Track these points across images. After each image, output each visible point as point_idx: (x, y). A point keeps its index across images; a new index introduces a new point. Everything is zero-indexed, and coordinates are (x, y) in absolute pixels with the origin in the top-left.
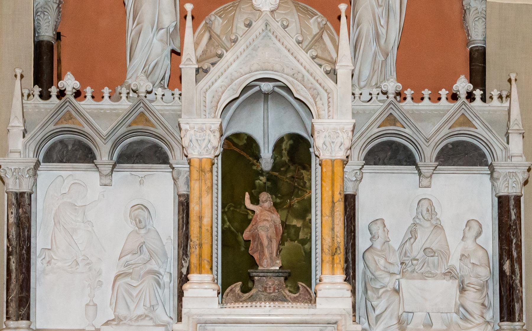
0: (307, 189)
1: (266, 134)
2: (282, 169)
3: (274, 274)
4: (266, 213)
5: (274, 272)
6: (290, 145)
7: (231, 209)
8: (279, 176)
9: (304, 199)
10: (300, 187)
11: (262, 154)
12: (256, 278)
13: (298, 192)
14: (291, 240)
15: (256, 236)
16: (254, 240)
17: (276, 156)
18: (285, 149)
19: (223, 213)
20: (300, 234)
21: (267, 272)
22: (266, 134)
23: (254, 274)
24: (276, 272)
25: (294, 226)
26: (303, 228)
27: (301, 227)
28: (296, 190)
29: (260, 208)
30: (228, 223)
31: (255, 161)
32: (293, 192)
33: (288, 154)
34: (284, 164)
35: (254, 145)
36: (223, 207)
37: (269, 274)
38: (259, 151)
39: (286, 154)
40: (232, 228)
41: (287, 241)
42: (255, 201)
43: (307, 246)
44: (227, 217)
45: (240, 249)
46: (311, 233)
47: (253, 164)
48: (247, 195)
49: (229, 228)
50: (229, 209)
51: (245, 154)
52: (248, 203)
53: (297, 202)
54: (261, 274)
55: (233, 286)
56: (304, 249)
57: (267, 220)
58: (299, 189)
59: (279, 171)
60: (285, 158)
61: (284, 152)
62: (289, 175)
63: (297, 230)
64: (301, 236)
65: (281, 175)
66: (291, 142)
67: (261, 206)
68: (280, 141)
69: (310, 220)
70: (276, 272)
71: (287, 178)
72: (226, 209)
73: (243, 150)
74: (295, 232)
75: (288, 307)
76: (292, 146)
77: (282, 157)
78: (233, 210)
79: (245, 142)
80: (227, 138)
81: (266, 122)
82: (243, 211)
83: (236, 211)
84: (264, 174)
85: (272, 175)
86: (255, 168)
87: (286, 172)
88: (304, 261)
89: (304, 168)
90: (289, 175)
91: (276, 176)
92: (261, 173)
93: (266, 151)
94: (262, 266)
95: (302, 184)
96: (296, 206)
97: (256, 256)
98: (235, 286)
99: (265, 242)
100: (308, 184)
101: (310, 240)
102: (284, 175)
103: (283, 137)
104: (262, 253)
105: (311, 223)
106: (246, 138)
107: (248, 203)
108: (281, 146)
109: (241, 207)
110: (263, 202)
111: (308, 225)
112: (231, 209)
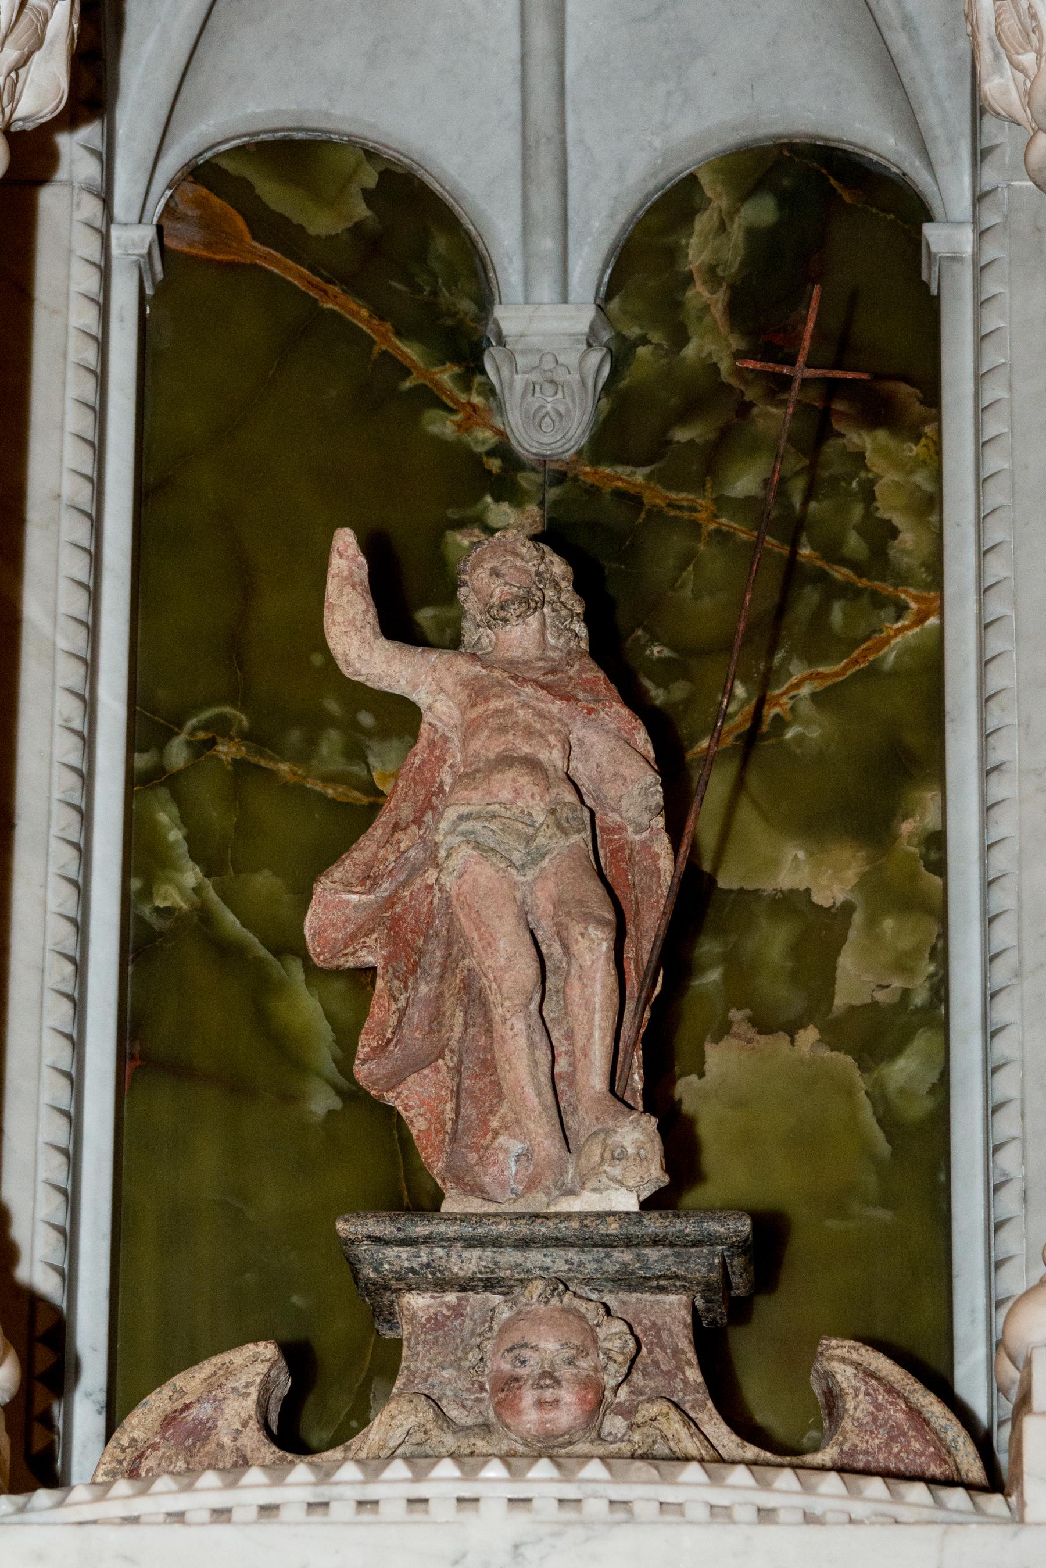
0: (902, 579)
1: (545, 152)
2: (681, 435)
3: (588, 1261)
4: (525, 702)
5: (588, 1235)
6: (751, 233)
7: (226, 750)
8: (657, 497)
9: (873, 672)
10: (840, 573)
11: (508, 317)
12: (418, 1303)
13: (822, 612)
14: (764, 1025)
15: (419, 934)
16: (407, 961)
17: (634, 332)
18: (711, 273)
19: (136, 783)
20: (847, 962)
21: (525, 1244)
22: (545, 152)
23: (398, 1257)
24: (608, 1243)
25: (793, 904)
26: (873, 921)
27: (848, 908)
28: (809, 597)
29: (465, 668)
30: (191, 876)
31: (446, 376)
32: (781, 610)
33: (733, 310)
34: (703, 394)
35: (441, 243)
36: (146, 728)
37: (535, 1257)
38: (485, 299)
39: (718, 311)
40: (231, 917)
41: (724, 1030)
42: (405, 607)
43: (904, 1070)
44: (185, 819)
45: (290, 1098)
46: (941, 954)
47: (429, 398)
48: (346, 556)
49: (204, 916)
50: (201, 749)
51: (359, 314)
52: (354, 640)
53: (815, 697)
54: (469, 1262)
55: (191, 1381)
56: (880, 1098)
57: (532, 764)
58: (833, 591)
59: (655, 452)
60: (712, 344)
61: (699, 293)
62: (745, 483)
63: (820, 933)
64: (856, 978)
65: (669, 480)
66: (762, 211)
67: (474, 657)
68: (674, 206)
69: (936, 842)
70: (608, 1243)
71: (722, 503)
72: (177, 755)
73: (350, 283)
74: (796, 950)
75: (718, 1513)
76: (763, 244)
77: (680, 336)
78: (240, 766)
79: (361, 211)
80: (202, 173)
81: (541, 36)
82: (328, 779)
83: (271, 774)
84: (526, 480)
85: (593, 491)
86: (442, 426)
87: (713, 460)
88: (884, 1202)
89: (879, 412)
90: (745, 483)
91: (630, 499)
92: (501, 473)
93: (545, 289)
94: (477, 1190)
95: (854, 544)
96: (808, 730)
97: (418, 1102)
98: (212, 1384)
99: (504, 962)
100: (909, 538)
101: (935, 1013)
102: (699, 486)
103: (690, 182)
104: (478, 1082)
105: (940, 868)
106: (370, 179)
107: (354, 640)
108: (673, 254)
109: (312, 742)
110: (497, 615)
111: (916, 887)
112: (226, 750)
